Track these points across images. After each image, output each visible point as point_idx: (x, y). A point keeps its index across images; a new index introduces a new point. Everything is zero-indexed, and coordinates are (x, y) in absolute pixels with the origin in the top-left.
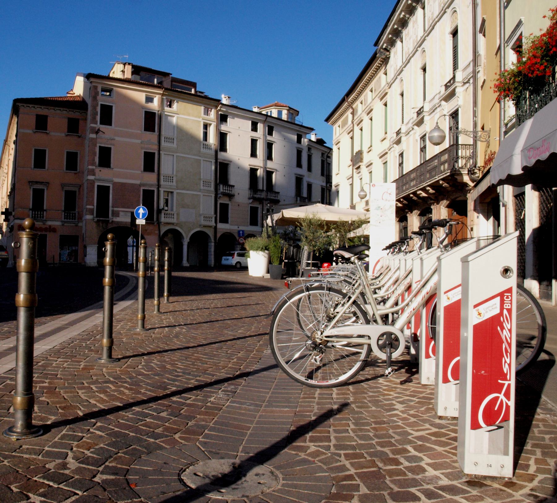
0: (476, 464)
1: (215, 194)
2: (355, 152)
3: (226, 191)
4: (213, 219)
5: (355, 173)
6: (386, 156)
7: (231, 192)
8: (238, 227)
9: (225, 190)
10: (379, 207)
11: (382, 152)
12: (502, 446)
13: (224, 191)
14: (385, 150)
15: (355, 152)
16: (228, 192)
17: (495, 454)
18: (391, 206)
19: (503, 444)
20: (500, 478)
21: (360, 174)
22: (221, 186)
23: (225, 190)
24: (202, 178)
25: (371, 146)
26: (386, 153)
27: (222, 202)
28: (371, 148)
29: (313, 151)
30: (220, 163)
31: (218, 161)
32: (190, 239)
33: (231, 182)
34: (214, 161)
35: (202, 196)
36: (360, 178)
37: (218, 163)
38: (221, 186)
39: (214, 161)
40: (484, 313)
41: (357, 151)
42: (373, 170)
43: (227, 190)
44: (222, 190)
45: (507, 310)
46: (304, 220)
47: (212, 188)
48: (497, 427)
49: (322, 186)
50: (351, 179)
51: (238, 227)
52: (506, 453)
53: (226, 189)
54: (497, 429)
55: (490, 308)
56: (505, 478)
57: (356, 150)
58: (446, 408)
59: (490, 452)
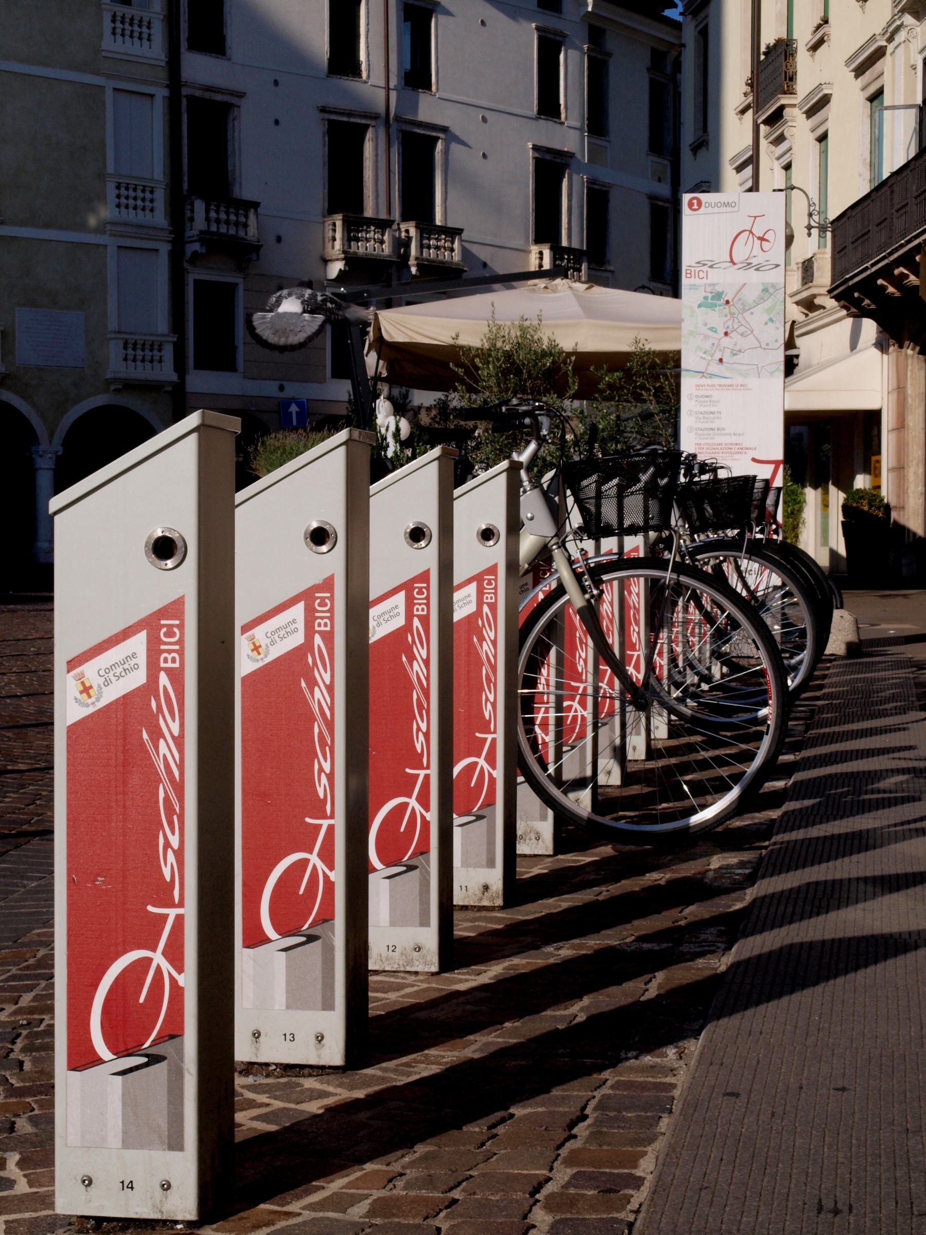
0: (88, 1182)
1: (173, 242)
2: (763, 49)
3: (223, 229)
4: (168, 353)
5: (764, 143)
6: (878, 66)
7: (241, 233)
8: (281, 388)
9: (218, 221)
10: (718, 296)
11: (862, 48)
12: (162, 1122)
13: (214, 228)
14: (873, 38)
15: (763, 49)
16: (232, 231)
17: (141, 1147)
18: (765, 290)
19: (165, 1112)
20: (164, 1222)
21: (784, 146)
22: (199, 206)
23: (218, 221)
24: (110, 169)
25: (826, 21)
26: (880, 53)
27: (204, 276)
28: (825, 29)
29: (612, 43)
30: (191, 99)
31: (185, 91)
32: (64, 444)
33: (247, 190)
34: (166, 92)
35: (112, 251)
36: (785, 161)
37: (184, 102)
38: (199, 206)
39: (161, 93)
40: (99, 686)
41: (772, 42)
42: (832, 127)
43: (227, 222)
44: (199, 224)
45: (170, 672)
46: (485, 355)
47: (160, 218)
48: (145, 1060)
49: (652, 198)
50: (749, 170)
51: (281, 388)
52: (176, 1144)
53: (223, 216)
54: (146, 1065)
55: (119, 670)
56: (176, 1222)
57: (768, 37)
58: (257, 1035)
59: (128, 1142)
